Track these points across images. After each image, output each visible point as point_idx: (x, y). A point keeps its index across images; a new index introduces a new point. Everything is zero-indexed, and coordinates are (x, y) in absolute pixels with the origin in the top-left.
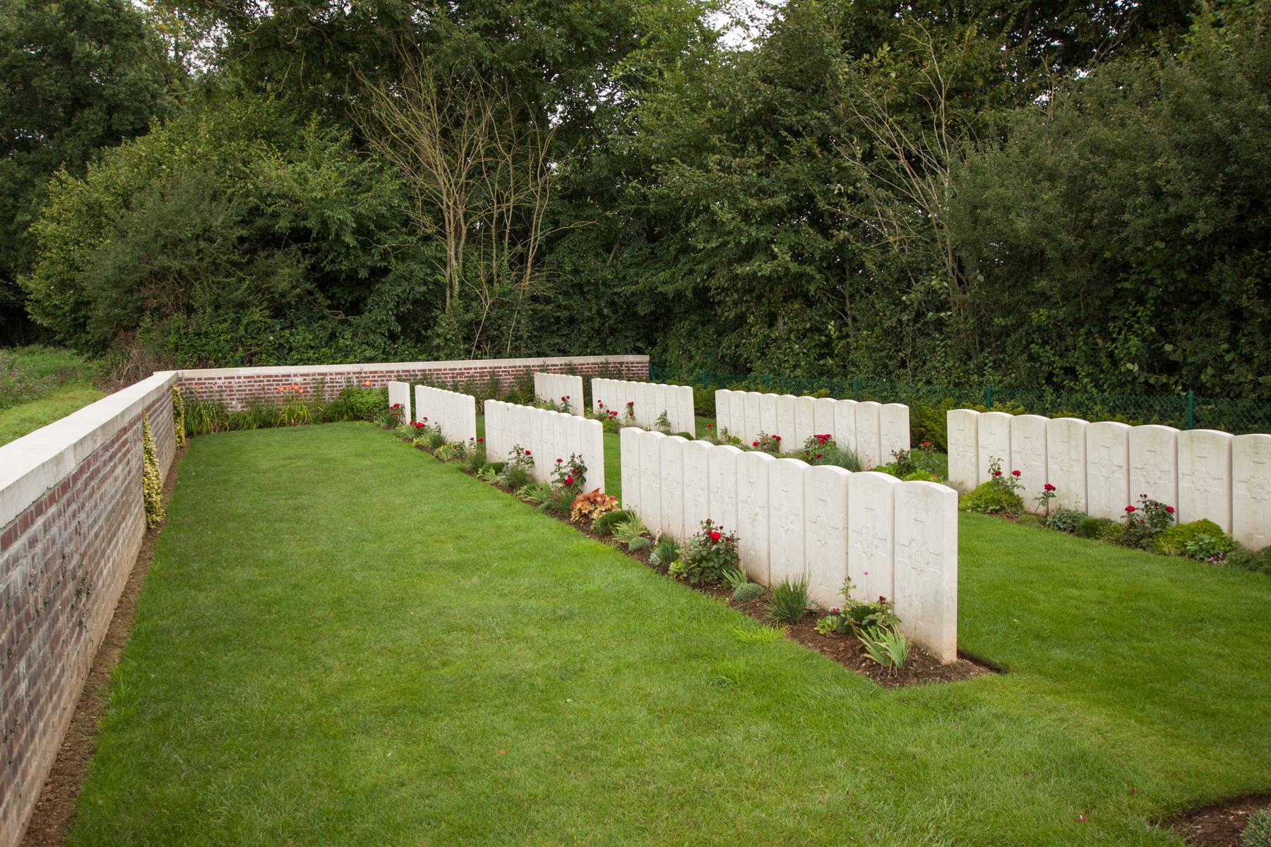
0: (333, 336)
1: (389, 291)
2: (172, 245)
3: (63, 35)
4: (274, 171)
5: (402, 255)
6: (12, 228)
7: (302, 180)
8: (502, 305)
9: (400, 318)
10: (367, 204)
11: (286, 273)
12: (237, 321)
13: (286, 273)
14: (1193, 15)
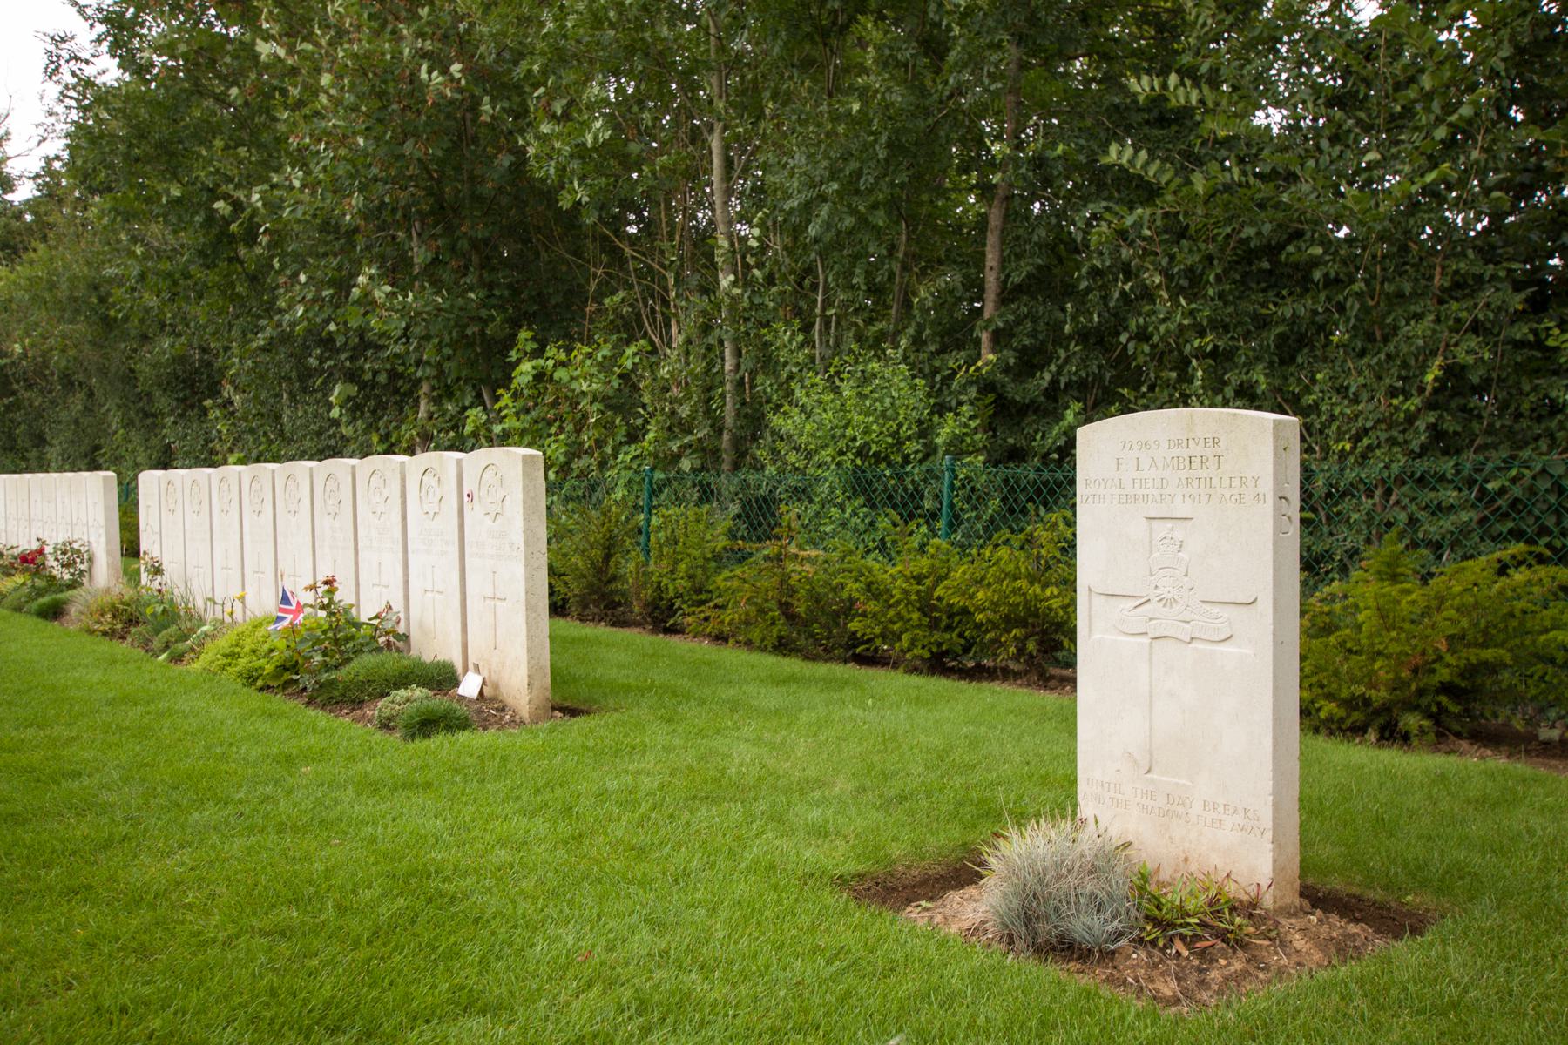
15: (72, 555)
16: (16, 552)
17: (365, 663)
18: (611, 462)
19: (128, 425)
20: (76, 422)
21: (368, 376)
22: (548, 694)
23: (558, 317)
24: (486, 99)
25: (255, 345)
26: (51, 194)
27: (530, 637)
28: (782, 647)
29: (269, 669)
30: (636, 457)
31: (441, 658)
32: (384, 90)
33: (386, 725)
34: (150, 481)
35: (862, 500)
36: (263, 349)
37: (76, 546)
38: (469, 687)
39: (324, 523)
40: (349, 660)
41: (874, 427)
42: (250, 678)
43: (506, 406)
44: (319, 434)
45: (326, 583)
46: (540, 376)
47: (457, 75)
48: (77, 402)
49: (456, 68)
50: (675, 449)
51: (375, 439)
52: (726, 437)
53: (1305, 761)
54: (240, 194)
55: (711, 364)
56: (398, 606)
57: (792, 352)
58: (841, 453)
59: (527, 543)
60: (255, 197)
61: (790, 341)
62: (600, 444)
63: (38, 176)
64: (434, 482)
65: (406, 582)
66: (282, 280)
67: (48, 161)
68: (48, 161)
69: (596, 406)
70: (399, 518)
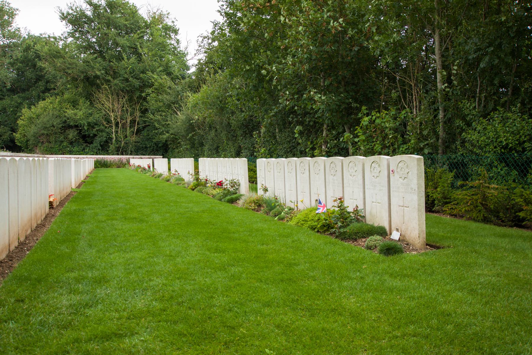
0: (84, 149)
1: (98, 140)
2: (45, 128)
3: (34, 60)
4: (70, 112)
5: (102, 131)
6: (16, 117)
7: (76, 114)
8: (127, 143)
9: (101, 146)
10: (91, 119)
11: (72, 134)
12: (60, 145)
13: (72, 134)
14: (9, 144)
15: (235, 184)
16: (215, 182)
17: (354, 226)
18: (397, 151)
19: (228, 139)
20: (212, 139)
21: (307, 123)
22: (425, 240)
23: (372, 101)
24: (350, 29)
25: (271, 114)
26: (200, 70)
27: (419, 221)
28: (486, 220)
29: (319, 226)
30: (406, 149)
31: (380, 225)
32: (318, 32)
33: (369, 248)
34: (261, 162)
35: (503, 164)
36: (273, 116)
37: (235, 181)
38: (396, 236)
39: (330, 178)
40: (348, 225)
41: (510, 138)
42: (313, 228)
43: (359, 132)
44: (289, 142)
45: (339, 199)
46: (372, 122)
47: (341, 22)
48: (213, 133)
49: (341, 20)
50: (422, 146)
51: (309, 143)
52: (440, 141)
53: (427, 219)
54: (269, 67)
55: (435, 117)
56: (361, 207)
57: (470, 110)
58: (495, 147)
59: (418, 188)
60: (274, 68)
61: (470, 106)
62: (393, 144)
63: (197, 65)
64: (377, 166)
65: (364, 199)
66: (281, 93)
67: (199, 60)
68: (199, 60)
69: (391, 132)
70: (362, 177)
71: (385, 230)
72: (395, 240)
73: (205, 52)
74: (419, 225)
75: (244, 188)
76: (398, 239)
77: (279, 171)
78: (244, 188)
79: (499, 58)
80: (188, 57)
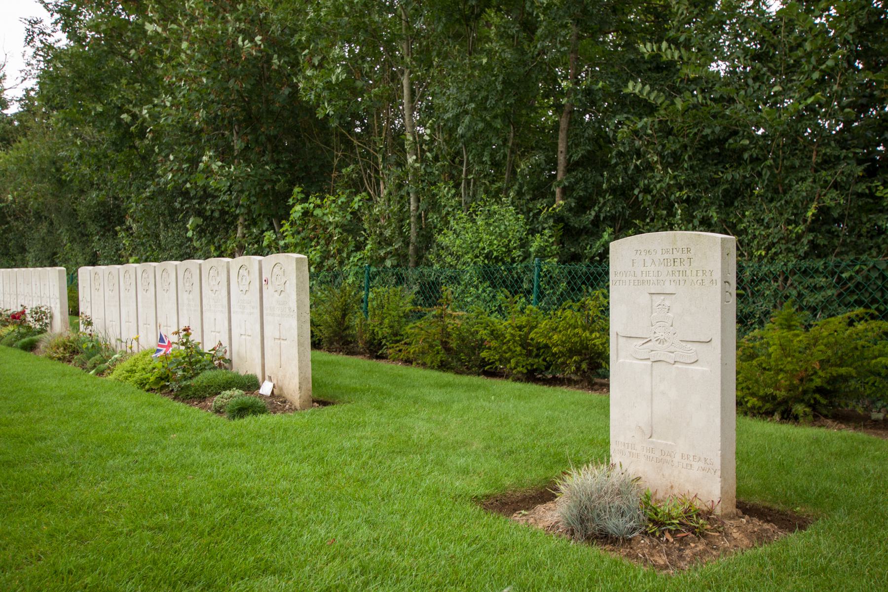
15: (41, 315)
16: (9, 313)
17: (206, 376)
18: (346, 262)
20: (43, 239)
21: (208, 213)
22: (310, 393)
23: (316, 180)
24: (275, 56)
25: (144, 195)
27: (300, 361)
28: (443, 366)
29: (152, 379)
30: (360, 259)
31: (249, 373)
33: (218, 411)
34: (85, 273)
35: (488, 283)
36: (149, 198)
37: (43, 309)
38: (266, 389)
39: (184, 296)
40: (197, 374)
41: (495, 242)
42: (142, 384)
43: (287, 230)
44: (180, 246)
45: (184, 330)
46: (306, 213)
47: (259, 43)
48: (44, 228)
49: (258, 38)
51: (212, 249)
52: (411, 247)
54: (136, 110)
56: (225, 344)
57: (448, 199)
58: (476, 257)
60: (145, 112)
62: (340, 251)
63: (21, 100)
64: (246, 273)
67: (27, 91)
68: (27, 91)
69: (337, 230)
70: (226, 294)
71: (256, 377)
72: (266, 397)
73: (38, 77)
74: (300, 368)
75: (59, 325)
76: (269, 393)
77: (111, 288)
78: (59, 325)
79: (483, 120)
80: (6, 84)
